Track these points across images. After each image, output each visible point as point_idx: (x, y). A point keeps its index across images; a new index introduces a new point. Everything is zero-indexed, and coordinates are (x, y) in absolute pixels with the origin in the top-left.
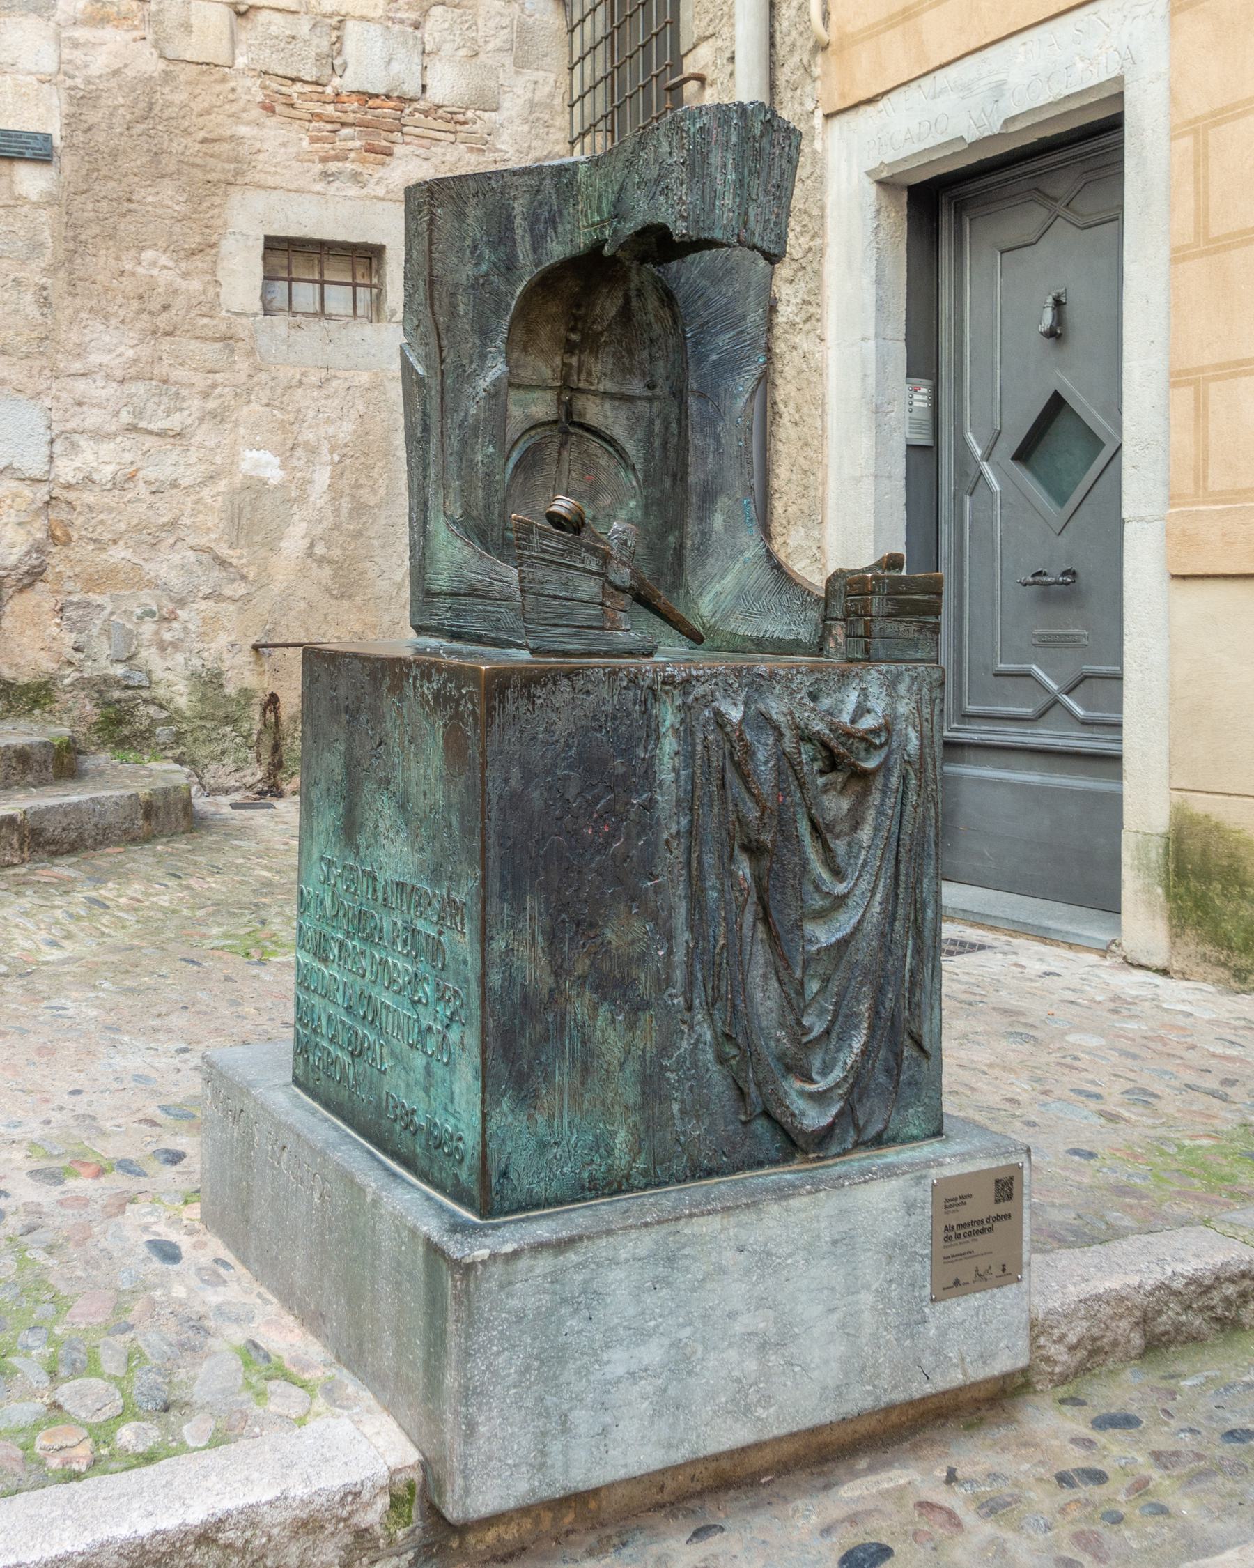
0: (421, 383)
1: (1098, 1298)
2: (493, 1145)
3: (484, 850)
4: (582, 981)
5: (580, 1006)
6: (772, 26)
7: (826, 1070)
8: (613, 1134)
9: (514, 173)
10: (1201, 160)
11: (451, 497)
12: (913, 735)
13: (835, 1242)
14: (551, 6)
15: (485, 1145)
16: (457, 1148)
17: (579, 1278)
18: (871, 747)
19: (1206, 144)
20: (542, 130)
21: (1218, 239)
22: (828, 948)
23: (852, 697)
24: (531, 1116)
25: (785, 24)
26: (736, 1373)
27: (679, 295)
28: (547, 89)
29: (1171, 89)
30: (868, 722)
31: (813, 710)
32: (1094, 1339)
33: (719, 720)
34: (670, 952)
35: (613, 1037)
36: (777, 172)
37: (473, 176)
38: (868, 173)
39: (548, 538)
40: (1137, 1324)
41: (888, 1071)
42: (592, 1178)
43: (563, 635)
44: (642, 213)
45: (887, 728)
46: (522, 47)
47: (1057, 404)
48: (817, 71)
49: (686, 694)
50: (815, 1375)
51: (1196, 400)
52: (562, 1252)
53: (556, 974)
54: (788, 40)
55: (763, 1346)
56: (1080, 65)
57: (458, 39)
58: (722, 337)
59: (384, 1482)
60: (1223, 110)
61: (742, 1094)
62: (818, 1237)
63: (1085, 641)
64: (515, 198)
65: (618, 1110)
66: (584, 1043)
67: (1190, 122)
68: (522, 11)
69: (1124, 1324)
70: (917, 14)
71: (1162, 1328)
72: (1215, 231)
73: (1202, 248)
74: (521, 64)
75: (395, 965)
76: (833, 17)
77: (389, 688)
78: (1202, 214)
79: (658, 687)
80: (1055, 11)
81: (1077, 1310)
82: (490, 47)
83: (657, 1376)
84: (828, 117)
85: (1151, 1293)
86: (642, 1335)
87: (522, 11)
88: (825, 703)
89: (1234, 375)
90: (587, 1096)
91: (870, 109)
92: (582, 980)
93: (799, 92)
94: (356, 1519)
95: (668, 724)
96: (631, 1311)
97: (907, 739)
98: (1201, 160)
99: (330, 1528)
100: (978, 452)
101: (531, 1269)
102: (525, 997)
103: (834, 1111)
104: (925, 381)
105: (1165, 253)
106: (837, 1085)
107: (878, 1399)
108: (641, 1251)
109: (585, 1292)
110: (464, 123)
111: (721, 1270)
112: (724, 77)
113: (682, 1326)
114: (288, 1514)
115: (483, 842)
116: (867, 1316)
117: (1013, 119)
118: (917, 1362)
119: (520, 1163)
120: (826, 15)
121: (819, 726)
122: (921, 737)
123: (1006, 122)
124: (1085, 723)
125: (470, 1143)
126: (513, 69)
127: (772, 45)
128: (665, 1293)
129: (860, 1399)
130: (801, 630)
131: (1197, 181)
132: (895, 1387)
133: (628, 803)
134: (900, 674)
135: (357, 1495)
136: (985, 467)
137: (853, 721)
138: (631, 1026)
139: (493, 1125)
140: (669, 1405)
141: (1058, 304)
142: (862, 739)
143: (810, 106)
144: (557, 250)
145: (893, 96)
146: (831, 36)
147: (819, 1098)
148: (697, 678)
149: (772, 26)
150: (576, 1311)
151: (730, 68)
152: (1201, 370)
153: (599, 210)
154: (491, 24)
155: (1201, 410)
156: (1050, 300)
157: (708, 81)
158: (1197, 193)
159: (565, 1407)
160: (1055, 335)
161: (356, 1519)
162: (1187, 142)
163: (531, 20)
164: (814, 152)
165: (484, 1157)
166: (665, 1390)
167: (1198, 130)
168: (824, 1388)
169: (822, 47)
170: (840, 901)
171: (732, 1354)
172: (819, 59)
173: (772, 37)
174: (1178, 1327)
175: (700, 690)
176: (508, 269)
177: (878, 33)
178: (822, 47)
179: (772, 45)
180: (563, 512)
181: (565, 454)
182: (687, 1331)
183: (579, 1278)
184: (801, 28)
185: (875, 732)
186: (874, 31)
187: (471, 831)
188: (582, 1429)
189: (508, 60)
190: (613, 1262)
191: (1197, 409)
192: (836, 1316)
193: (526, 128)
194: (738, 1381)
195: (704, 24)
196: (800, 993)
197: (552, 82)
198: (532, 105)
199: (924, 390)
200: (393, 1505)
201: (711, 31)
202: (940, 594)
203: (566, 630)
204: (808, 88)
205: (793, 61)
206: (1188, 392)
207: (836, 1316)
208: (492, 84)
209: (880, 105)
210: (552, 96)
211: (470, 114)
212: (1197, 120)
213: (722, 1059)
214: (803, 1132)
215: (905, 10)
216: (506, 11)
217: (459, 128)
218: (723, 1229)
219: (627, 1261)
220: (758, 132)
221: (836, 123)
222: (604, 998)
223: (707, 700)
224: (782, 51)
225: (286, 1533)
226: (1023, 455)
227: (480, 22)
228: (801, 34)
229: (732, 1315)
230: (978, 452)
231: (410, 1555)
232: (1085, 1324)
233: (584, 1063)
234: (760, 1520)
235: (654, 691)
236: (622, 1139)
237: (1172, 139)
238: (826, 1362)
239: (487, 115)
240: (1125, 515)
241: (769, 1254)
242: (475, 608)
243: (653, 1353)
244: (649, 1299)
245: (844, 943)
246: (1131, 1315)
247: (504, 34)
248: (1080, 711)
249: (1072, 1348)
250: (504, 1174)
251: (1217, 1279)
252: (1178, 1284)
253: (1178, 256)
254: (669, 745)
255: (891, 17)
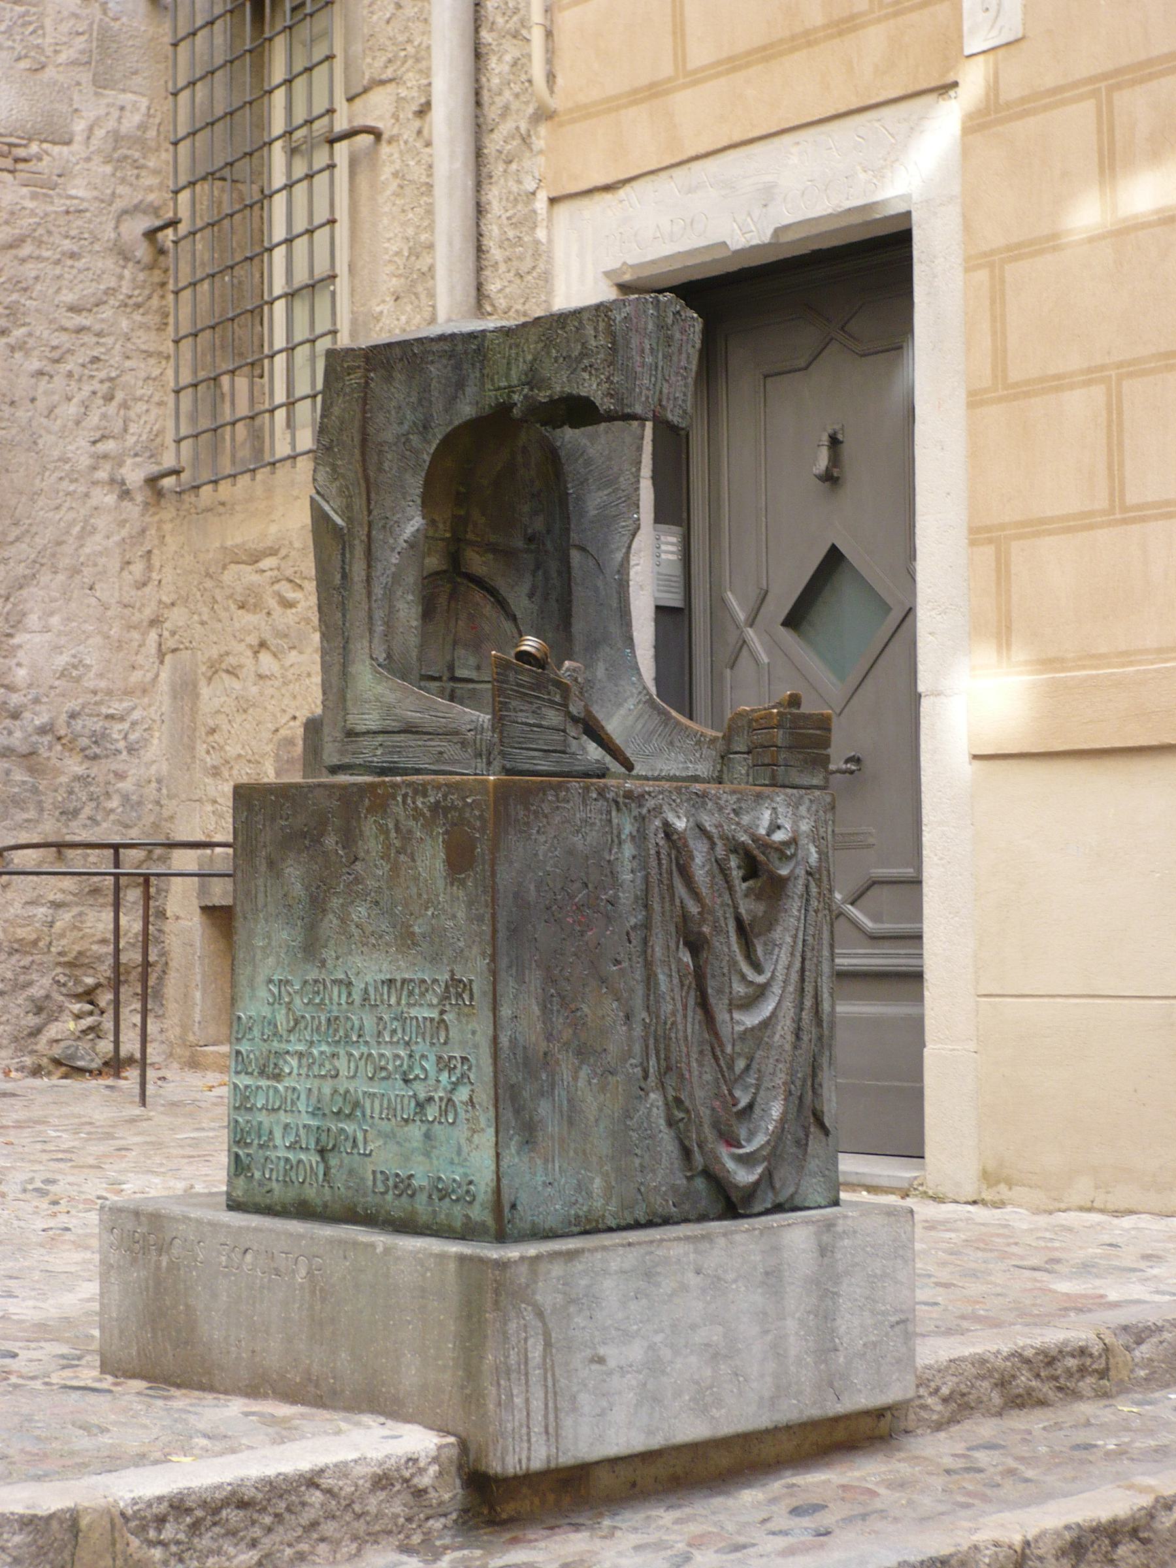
0: (336, 530)
1: (963, 1359)
2: (504, 1182)
3: (495, 931)
4: (567, 1045)
5: (566, 1064)
6: (477, 80)
7: (752, 1135)
8: (592, 1179)
9: (432, 340)
10: (997, 297)
11: (376, 641)
12: (813, 850)
13: (767, 1274)
14: (143, 7)
15: (498, 1179)
16: (468, 1192)
17: (583, 1282)
18: (784, 858)
19: (1003, 281)
20: (131, 172)
21: (1016, 385)
22: (753, 1029)
23: (767, 815)
24: (532, 1158)
25: (496, 81)
26: (696, 1377)
27: (562, 453)
28: (137, 118)
29: (964, 216)
30: (779, 836)
31: (738, 824)
32: (963, 1395)
33: (668, 831)
34: (630, 1029)
35: (590, 1099)
36: (684, 355)
37: (398, 343)
38: (607, 274)
39: (521, 673)
40: (996, 1385)
41: (798, 1142)
42: (577, 1216)
43: (534, 758)
44: (560, 384)
45: (794, 841)
46: (103, 61)
47: (834, 559)
48: (539, 143)
49: (640, 806)
50: (755, 1385)
51: (998, 560)
52: (571, 1260)
53: (548, 1041)
54: (500, 101)
55: (715, 1356)
56: (862, 176)
57: (18, 47)
58: (600, 493)
59: (434, 1453)
60: (1019, 245)
61: (686, 1153)
62: (755, 1268)
63: (871, 840)
64: (432, 362)
65: (594, 1159)
66: (569, 1101)
67: (984, 255)
68: (105, 12)
69: (986, 1384)
70: (667, 92)
71: (1017, 1391)
72: (1014, 376)
73: (1001, 393)
74: (102, 83)
75: (382, 1055)
76: (560, 80)
77: (368, 811)
78: (1000, 356)
79: (620, 800)
80: (831, 112)
81: (948, 1368)
82: (62, 58)
83: (639, 1372)
84: (553, 201)
85: (1007, 1359)
86: (627, 1336)
87: (105, 12)
88: (746, 819)
89: (1037, 534)
90: (573, 1145)
91: (608, 197)
92: (567, 1045)
93: (514, 166)
94: (415, 1481)
95: (627, 832)
96: (620, 1315)
97: (809, 853)
98: (997, 297)
99: (398, 1487)
100: (741, 616)
101: (549, 1272)
102: (526, 1058)
103: (759, 1170)
104: (674, 528)
105: (961, 395)
106: (762, 1147)
107: (801, 1411)
108: (626, 1266)
109: (586, 1295)
110: (25, 160)
111: (684, 1288)
112: (408, 134)
113: (656, 1332)
114: (370, 1470)
115: (494, 925)
116: (792, 1339)
117: (787, 228)
118: (831, 1385)
119: (524, 1199)
120: (551, 77)
121: (744, 838)
122: (819, 852)
123: (777, 231)
124: (875, 938)
125: (482, 1188)
126: (92, 89)
127: (478, 104)
128: (644, 1301)
129: (790, 1411)
130: (699, 767)
131: (993, 319)
132: (815, 1403)
133: (598, 898)
134: (801, 797)
135: (416, 1461)
136: (750, 633)
137: (768, 835)
138: (603, 1089)
139: (504, 1164)
140: (651, 1399)
141: (835, 442)
142: (777, 849)
143: (530, 185)
144: (467, 410)
145: (634, 184)
146: (553, 103)
147: (746, 1160)
148: (649, 793)
149: (477, 80)
150: (580, 1310)
151: (417, 123)
152: (1002, 527)
153: (507, 376)
154: (65, 27)
155: (1003, 570)
156: (825, 439)
157: (385, 136)
158: (994, 333)
159: (575, 1389)
160: (831, 478)
161: (415, 1481)
162: (983, 275)
163: (116, 25)
164: (537, 242)
165: (498, 1191)
166: (645, 1384)
167: (992, 263)
168: (761, 1398)
169: (543, 115)
170: (761, 992)
171: (693, 1359)
172: (543, 129)
173: (477, 93)
174: (1029, 1391)
175: (651, 803)
176: (425, 427)
177: (618, 108)
178: (543, 115)
179: (478, 104)
180: (532, 650)
181: (453, 605)
182: (659, 1338)
183: (583, 1282)
184: (517, 88)
185: (784, 843)
186: (612, 105)
187: (480, 919)
188: (587, 1409)
189: (86, 77)
190: (605, 1272)
191: (998, 571)
192: (769, 1337)
193: (108, 169)
194: (697, 1383)
195: (379, 63)
196: (731, 1068)
197: (143, 109)
198: (117, 138)
199: (674, 540)
200: (440, 1473)
201: (389, 73)
202: (829, 730)
203: (536, 754)
204: (526, 164)
205: (506, 128)
206: (990, 550)
207: (769, 1337)
208: (64, 108)
209: (621, 193)
210: (143, 127)
211: (34, 148)
212: (992, 252)
213: (671, 1123)
214: (736, 1187)
215: (652, 85)
216: (84, 12)
217: (20, 166)
218: (686, 1254)
219: (616, 1273)
220: (670, 321)
221: (562, 209)
222: (582, 1062)
223: (658, 810)
224: (492, 112)
225: (368, 1485)
226: (795, 620)
227: (48, 23)
228: (517, 96)
229: (694, 1327)
230: (741, 616)
231: (454, 1516)
232: (955, 1379)
233: (570, 1117)
234: (718, 1501)
235: (617, 803)
236: (597, 1184)
237: (967, 270)
238: (762, 1376)
239: (56, 150)
240: (921, 688)
241: (719, 1279)
242: (412, 743)
243: (635, 1352)
244: (633, 1306)
245: (766, 1024)
246: (991, 1376)
247: (80, 42)
248: (869, 924)
249: (945, 1400)
250: (513, 1206)
251: (1061, 1352)
252: (1029, 1353)
253: (975, 400)
254: (628, 850)
255: (635, 91)
